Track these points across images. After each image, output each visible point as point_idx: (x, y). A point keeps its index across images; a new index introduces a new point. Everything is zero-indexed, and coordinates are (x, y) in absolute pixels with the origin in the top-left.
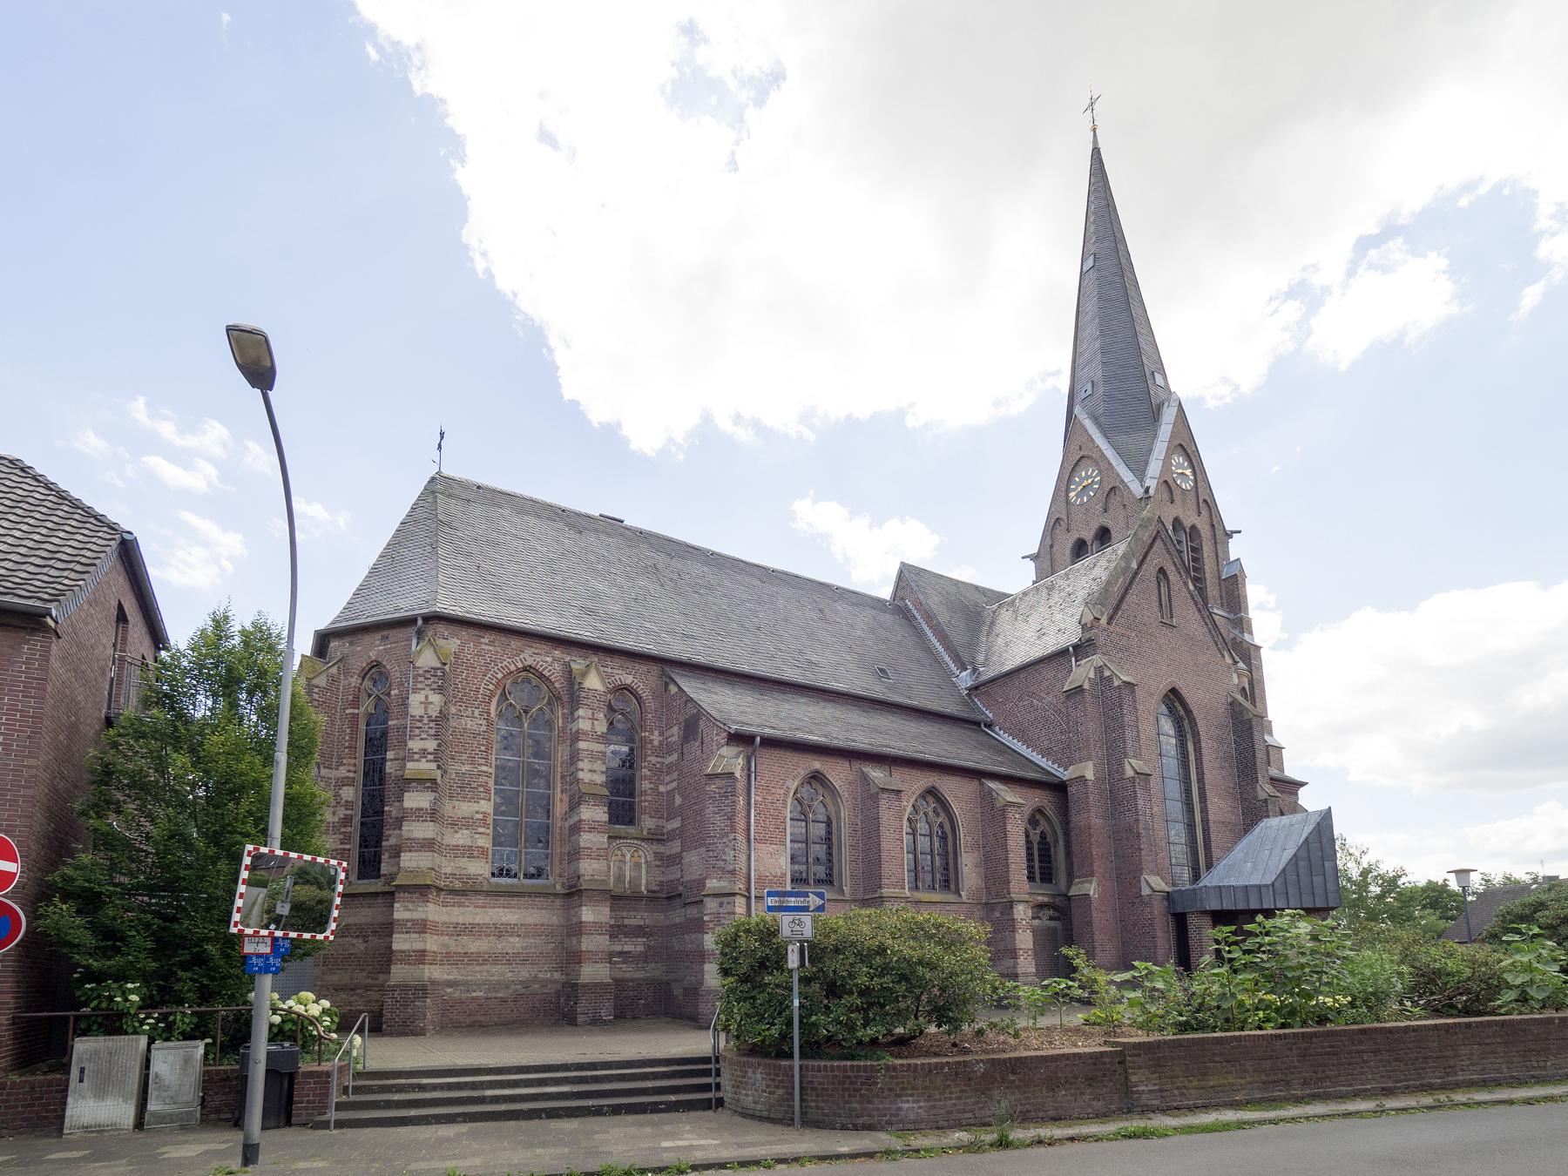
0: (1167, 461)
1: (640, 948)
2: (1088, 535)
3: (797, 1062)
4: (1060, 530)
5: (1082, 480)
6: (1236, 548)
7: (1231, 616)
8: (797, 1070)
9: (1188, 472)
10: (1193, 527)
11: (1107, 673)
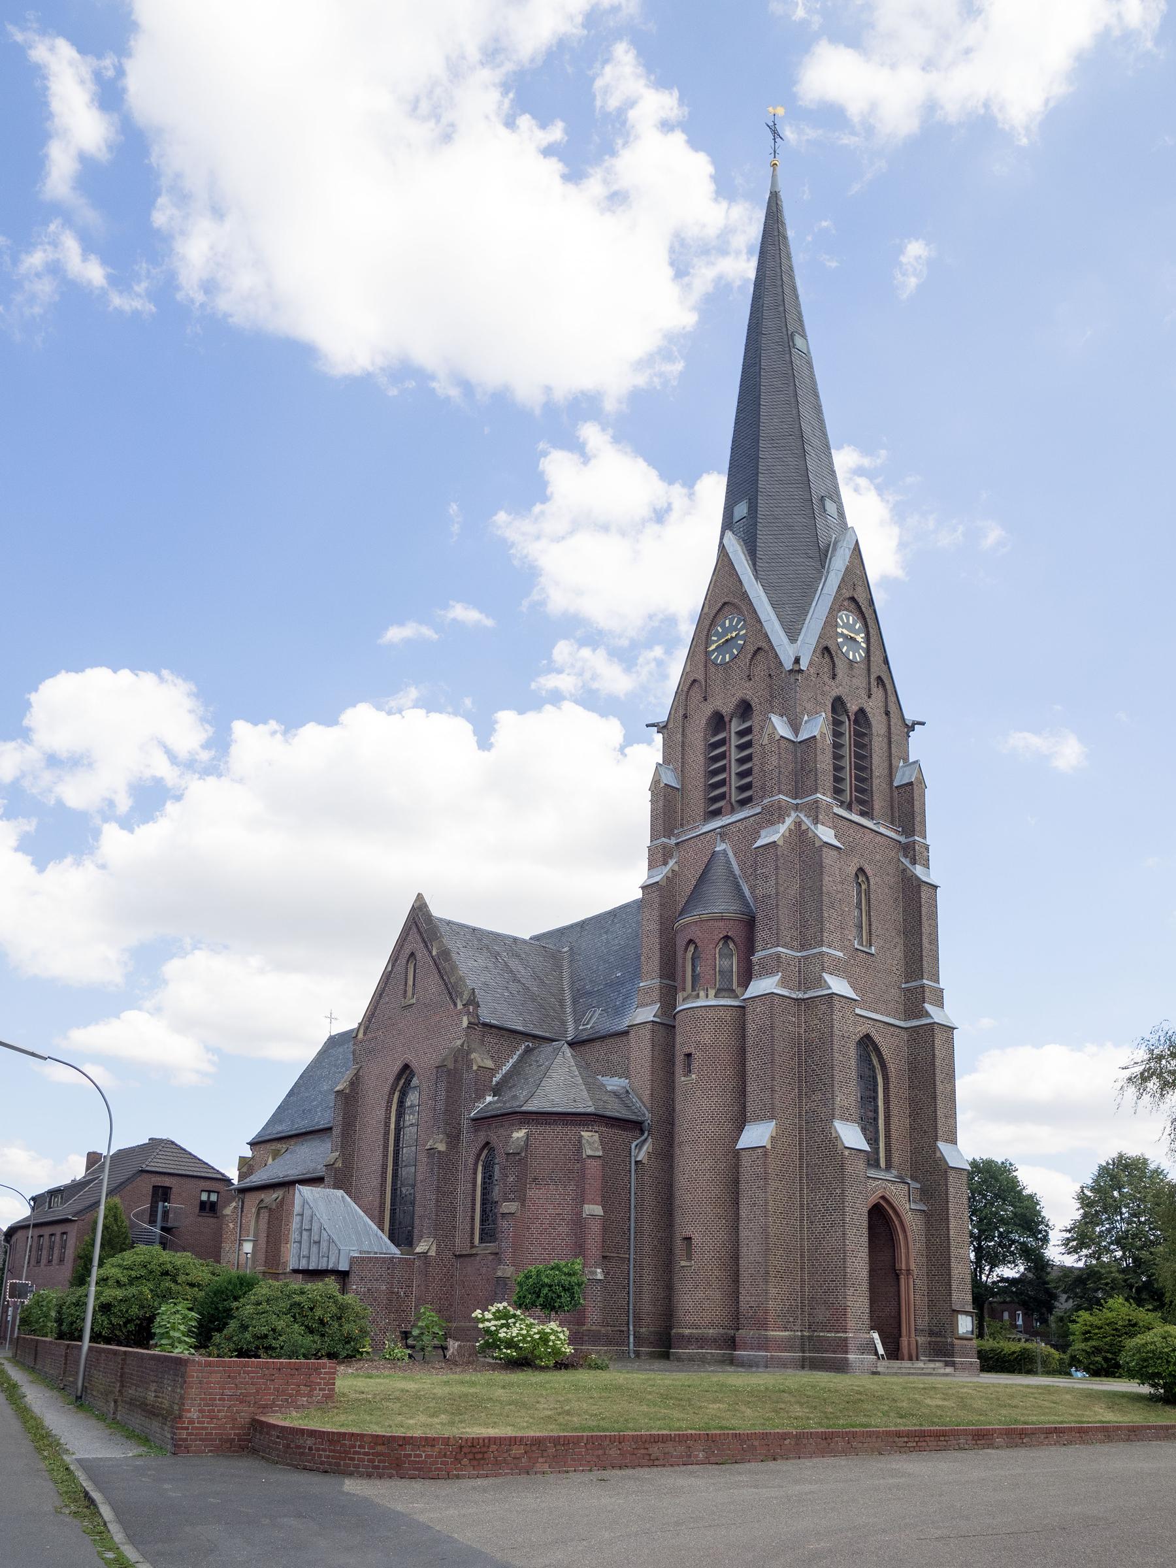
0: (830, 623)
1: (349, 1380)
2: (726, 709)
3: (86, 1343)
4: (696, 694)
5: (726, 631)
6: (918, 746)
7: (902, 839)
8: (631, 1345)
9: (860, 638)
10: (862, 711)
11: (804, 827)
